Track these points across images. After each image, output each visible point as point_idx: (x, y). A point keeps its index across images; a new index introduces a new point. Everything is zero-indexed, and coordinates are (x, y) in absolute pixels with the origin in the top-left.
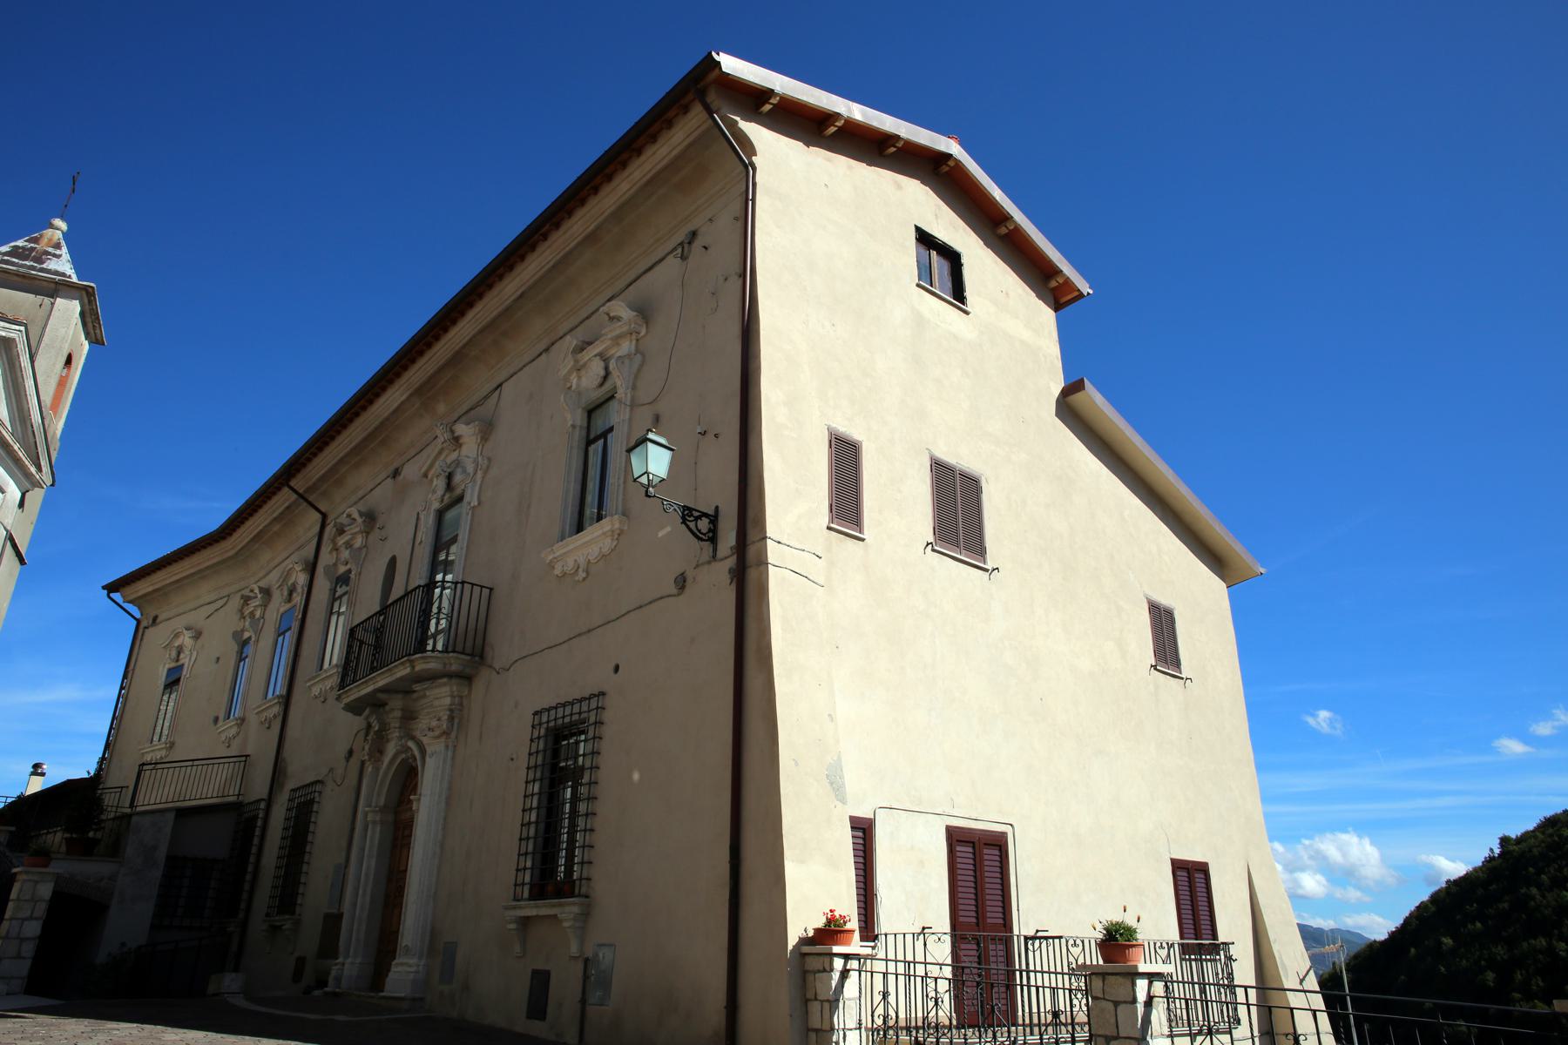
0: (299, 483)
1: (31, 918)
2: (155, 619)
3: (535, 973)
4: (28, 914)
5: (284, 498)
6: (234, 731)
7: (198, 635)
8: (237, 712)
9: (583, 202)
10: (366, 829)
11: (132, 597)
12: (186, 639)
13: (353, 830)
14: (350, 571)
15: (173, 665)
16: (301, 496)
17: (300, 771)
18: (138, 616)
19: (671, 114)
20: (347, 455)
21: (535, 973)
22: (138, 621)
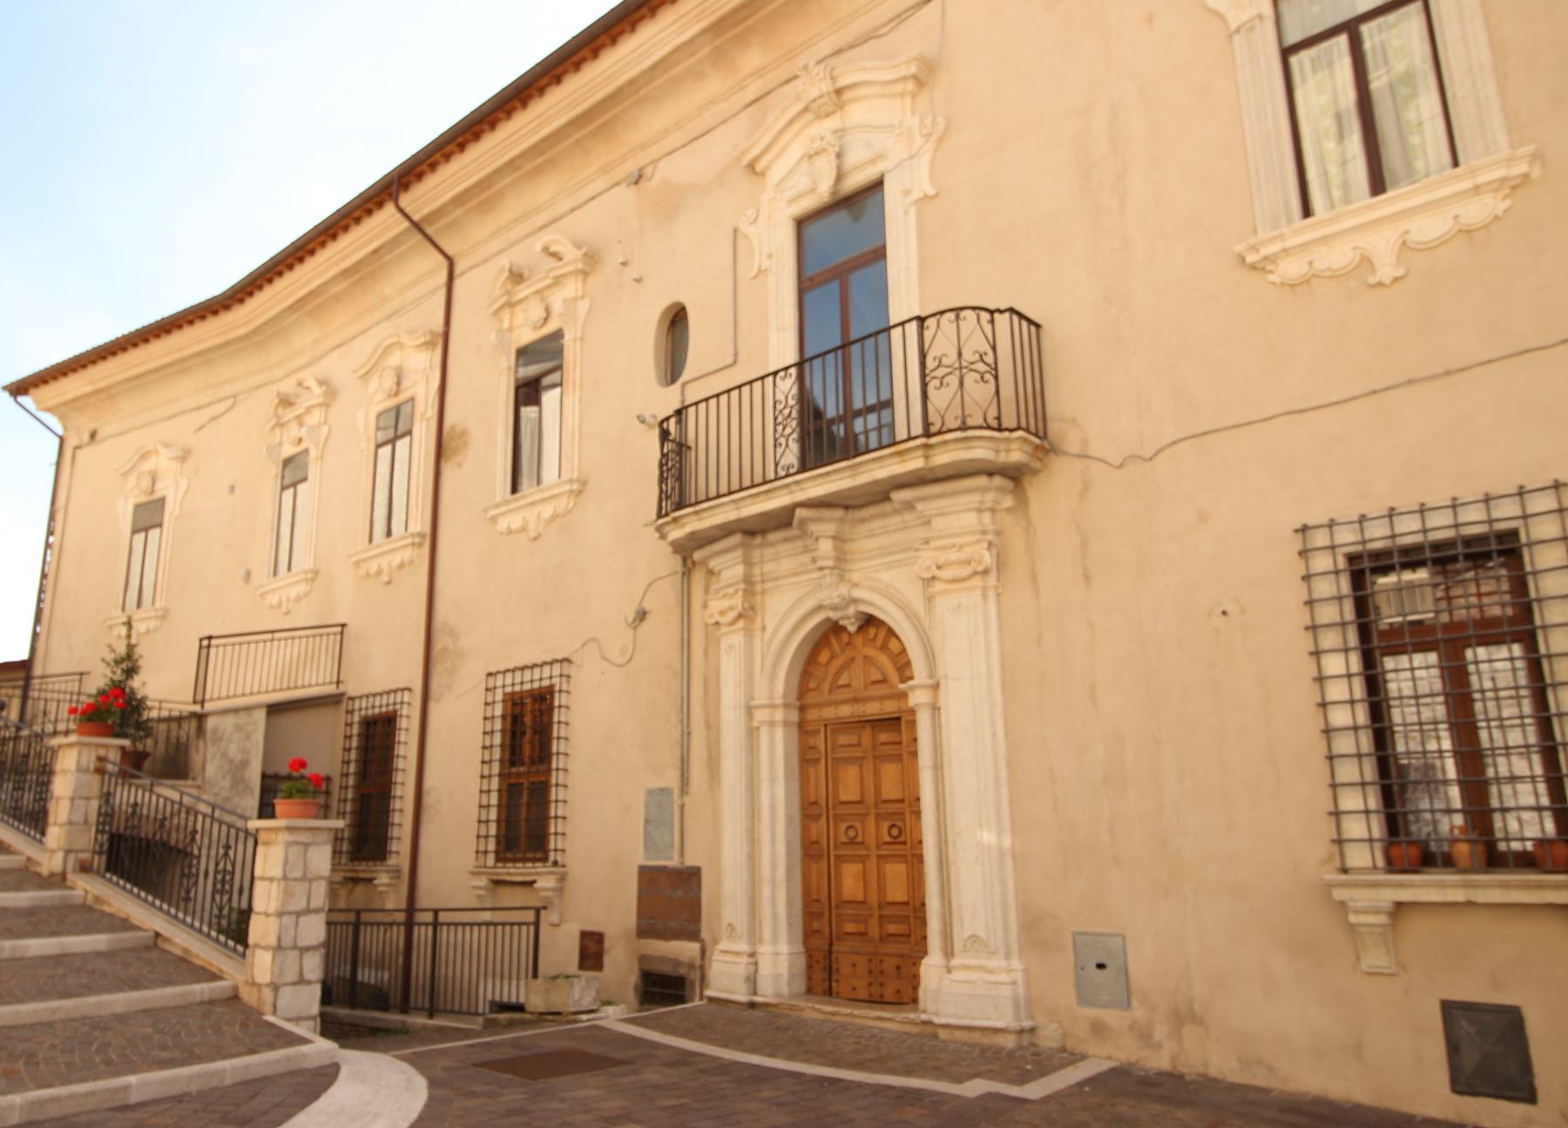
0: (419, 199)
1: (308, 911)
2: (93, 435)
3: (585, 935)
4: (302, 905)
5: (386, 221)
6: (301, 589)
7: (185, 456)
8: (303, 561)
9: (577, 67)
10: (752, 733)
11: (52, 402)
12: (163, 462)
13: (686, 734)
14: (306, 451)
15: (143, 499)
16: (417, 226)
17: (496, 643)
18: (60, 431)
19: (543, 82)
20: (523, 155)
21: (585, 935)
22: (62, 439)
